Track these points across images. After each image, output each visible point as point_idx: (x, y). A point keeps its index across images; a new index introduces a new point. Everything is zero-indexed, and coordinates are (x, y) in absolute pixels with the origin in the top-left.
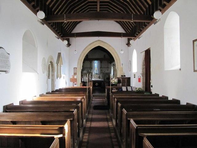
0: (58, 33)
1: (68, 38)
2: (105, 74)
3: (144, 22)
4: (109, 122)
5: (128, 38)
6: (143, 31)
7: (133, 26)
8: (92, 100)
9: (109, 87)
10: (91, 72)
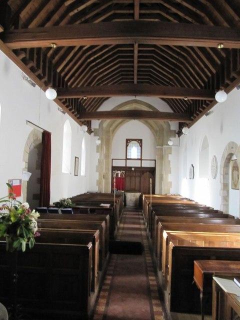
0: (32, 70)
1: (88, 120)
3: (205, 101)
4: (155, 283)
5: (179, 123)
6: (197, 118)
7: (210, 75)
8: (123, 214)
9: (149, 196)
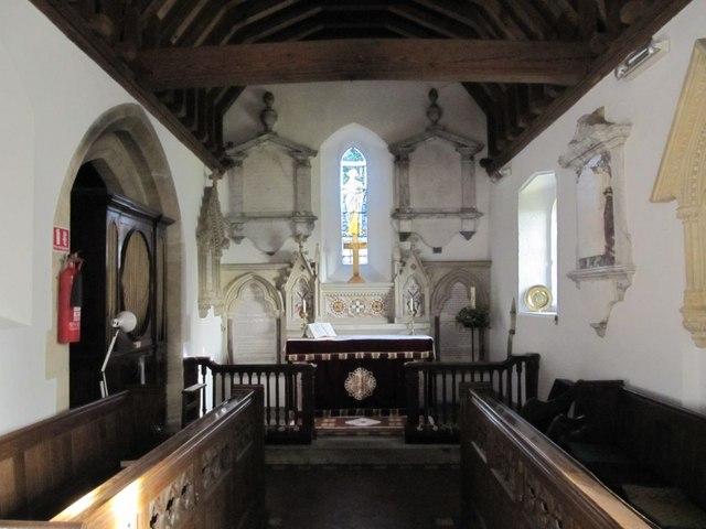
2: (440, 273)
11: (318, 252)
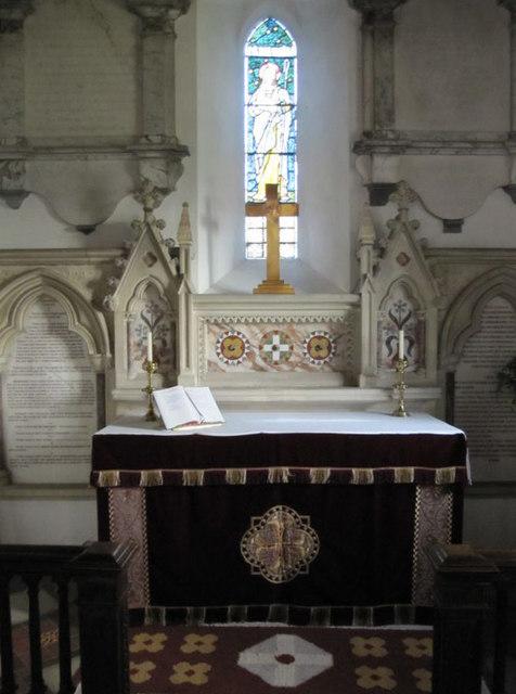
10: (150, 228)
11: (185, 223)
